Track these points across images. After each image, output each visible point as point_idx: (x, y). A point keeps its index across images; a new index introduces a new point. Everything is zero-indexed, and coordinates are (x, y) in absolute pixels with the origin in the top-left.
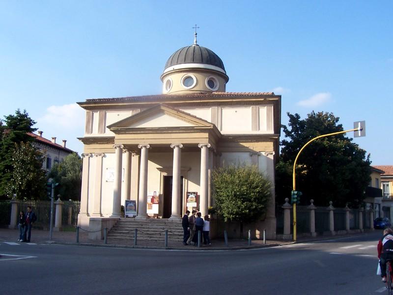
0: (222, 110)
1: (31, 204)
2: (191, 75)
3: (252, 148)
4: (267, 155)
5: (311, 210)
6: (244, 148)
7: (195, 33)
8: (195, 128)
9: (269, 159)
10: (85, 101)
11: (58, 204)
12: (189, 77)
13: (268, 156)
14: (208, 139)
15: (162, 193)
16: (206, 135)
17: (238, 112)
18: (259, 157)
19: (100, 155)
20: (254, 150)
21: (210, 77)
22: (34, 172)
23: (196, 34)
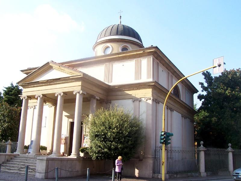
0: (112, 65)
1: (126, 145)
2: (108, 44)
3: (134, 95)
4: (147, 100)
5: (200, 151)
6: (128, 96)
7: (120, 16)
8: (70, 78)
9: (148, 104)
10: (26, 69)
11: (8, 144)
12: (108, 47)
13: (147, 102)
14: (81, 87)
15: (68, 136)
16: (79, 83)
17: (124, 66)
18: (140, 102)
19: (32, 107)
20: (136, 97)
21: (123, 45)
22: (8, 122)
23: (121, 17)
